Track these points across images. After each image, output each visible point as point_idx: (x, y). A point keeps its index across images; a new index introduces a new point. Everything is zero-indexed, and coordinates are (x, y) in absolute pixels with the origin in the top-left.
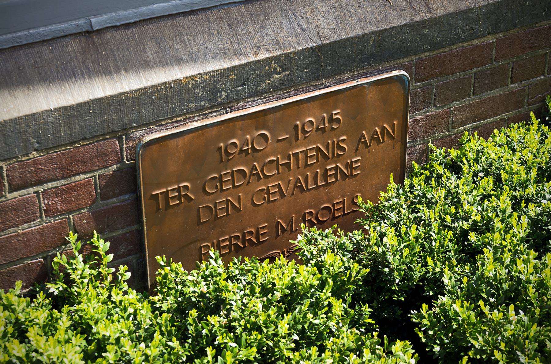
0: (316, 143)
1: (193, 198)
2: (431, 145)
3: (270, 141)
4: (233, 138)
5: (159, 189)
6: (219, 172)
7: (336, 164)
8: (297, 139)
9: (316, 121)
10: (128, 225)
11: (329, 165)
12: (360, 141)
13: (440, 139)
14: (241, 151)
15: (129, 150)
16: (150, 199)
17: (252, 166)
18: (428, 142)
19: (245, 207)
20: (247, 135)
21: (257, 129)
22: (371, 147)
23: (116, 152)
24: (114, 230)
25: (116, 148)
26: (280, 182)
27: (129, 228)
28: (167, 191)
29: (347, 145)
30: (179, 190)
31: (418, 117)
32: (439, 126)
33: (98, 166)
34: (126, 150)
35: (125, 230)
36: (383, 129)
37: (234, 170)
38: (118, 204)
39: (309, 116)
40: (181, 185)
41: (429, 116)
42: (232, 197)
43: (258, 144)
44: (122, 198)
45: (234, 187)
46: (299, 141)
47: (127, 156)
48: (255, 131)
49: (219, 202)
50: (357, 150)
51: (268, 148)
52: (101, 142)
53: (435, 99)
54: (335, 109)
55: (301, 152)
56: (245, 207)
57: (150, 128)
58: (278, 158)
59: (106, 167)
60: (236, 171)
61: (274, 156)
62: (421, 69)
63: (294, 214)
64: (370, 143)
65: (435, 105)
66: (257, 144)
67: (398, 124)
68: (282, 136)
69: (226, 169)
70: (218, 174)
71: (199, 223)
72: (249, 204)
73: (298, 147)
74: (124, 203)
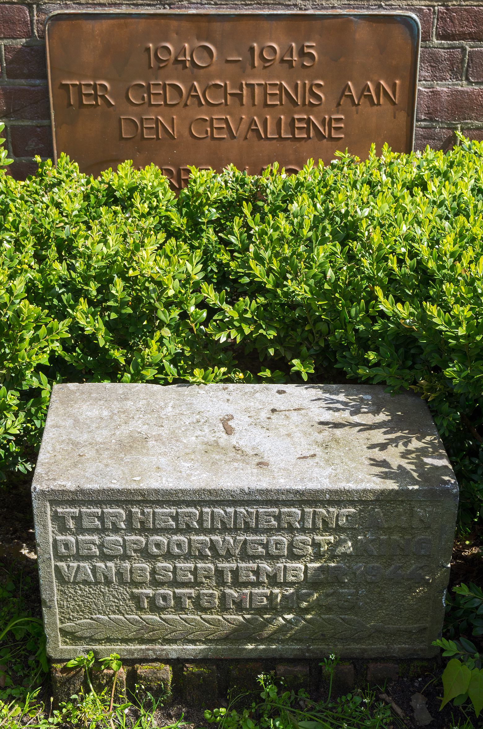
0: (278, 78)
1: (113, 103)
2: (459, 133)
3: (215, 58)
4: (167, 40)
5: (71, 79)
6: (147, 80)
7: (308, 115)
8: (253, 66)
9: (280, 49)
10: (38, 117)
11: (299, 113)
12: (343, 94)
13: (474, 129)
14: (176, 61)
15: (41, 24)
16: (59, 88)
17: (190, 84)
18: (456, 129)
19: (180, 135)
20: (185, 42)
21: (199, 38)
22: (360, 107)
23: (25, 22)
24: (22, 118)
25: (24, 18)
26: (228, 117)
27: (40, 121)
28: (80, 84)
29: (324, 94)
30: (95, 87)
31: (439, 88)
32: (472, 110)
33: (4, 34)
34: (37, 23)
35: (35, 123)
36: (378, 87)
37: (167, 82)
38: (27, 87)
39: (271, 40)
40: (98, 82)
41: (457, 91)
42: (163, 117)
43: (200, 59)
44: (32, 82)
45: (166, 104)
46: (255, 70)
47: (38, 31)
48: (196, 41)
49: (146, 119)
50: (339, 104)
51: (212, 68)
52: (7, 5)
53: (467, 71)
54: (308, 40)
55: (258, 84)
56: (180, 135)
57: (66, 4)
58: (226, 84)
59: (14, 38)
60: (169, 84)
61: (221, 80)
62: (446, 21)
63: (248, 165)
64: (359, 101)
65: (467, 79)
66: (197, 58)
67: (402, 85)
68: (233, 57)
69: (156, 79)
70: (146, 82)
71: (121, 138)
72: (186, 133)
73: (254, 77)
74: (33, 88)
